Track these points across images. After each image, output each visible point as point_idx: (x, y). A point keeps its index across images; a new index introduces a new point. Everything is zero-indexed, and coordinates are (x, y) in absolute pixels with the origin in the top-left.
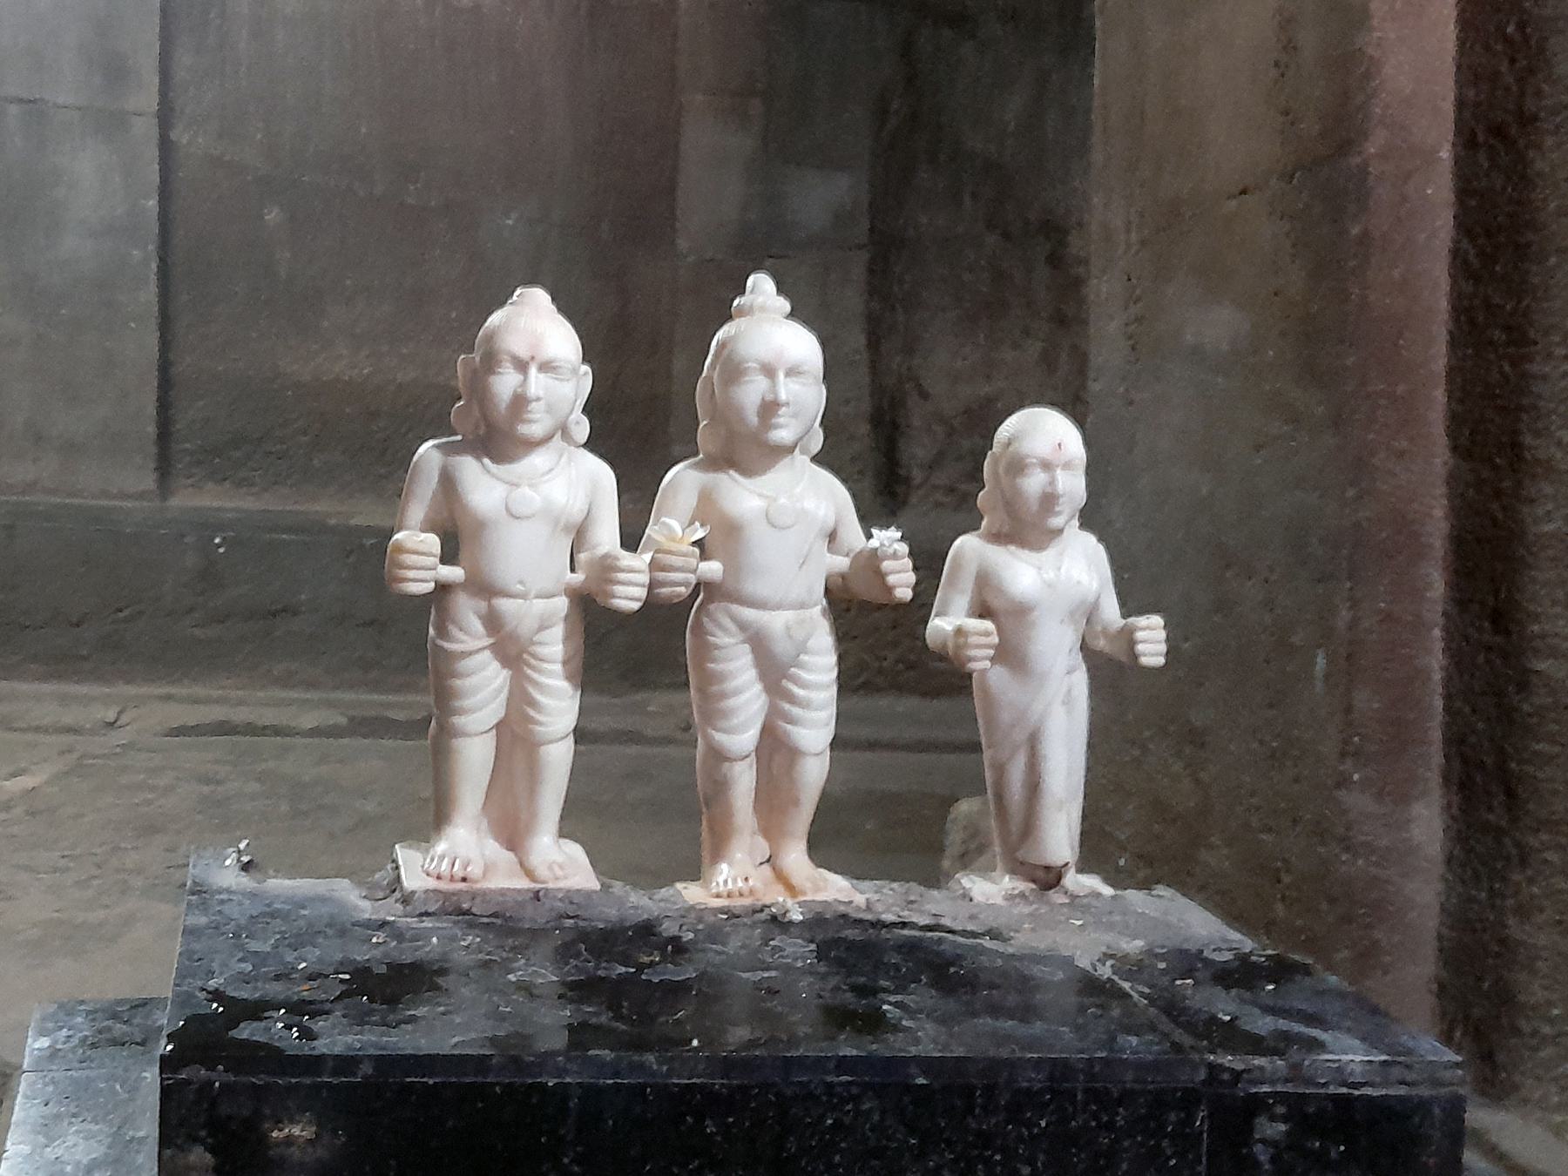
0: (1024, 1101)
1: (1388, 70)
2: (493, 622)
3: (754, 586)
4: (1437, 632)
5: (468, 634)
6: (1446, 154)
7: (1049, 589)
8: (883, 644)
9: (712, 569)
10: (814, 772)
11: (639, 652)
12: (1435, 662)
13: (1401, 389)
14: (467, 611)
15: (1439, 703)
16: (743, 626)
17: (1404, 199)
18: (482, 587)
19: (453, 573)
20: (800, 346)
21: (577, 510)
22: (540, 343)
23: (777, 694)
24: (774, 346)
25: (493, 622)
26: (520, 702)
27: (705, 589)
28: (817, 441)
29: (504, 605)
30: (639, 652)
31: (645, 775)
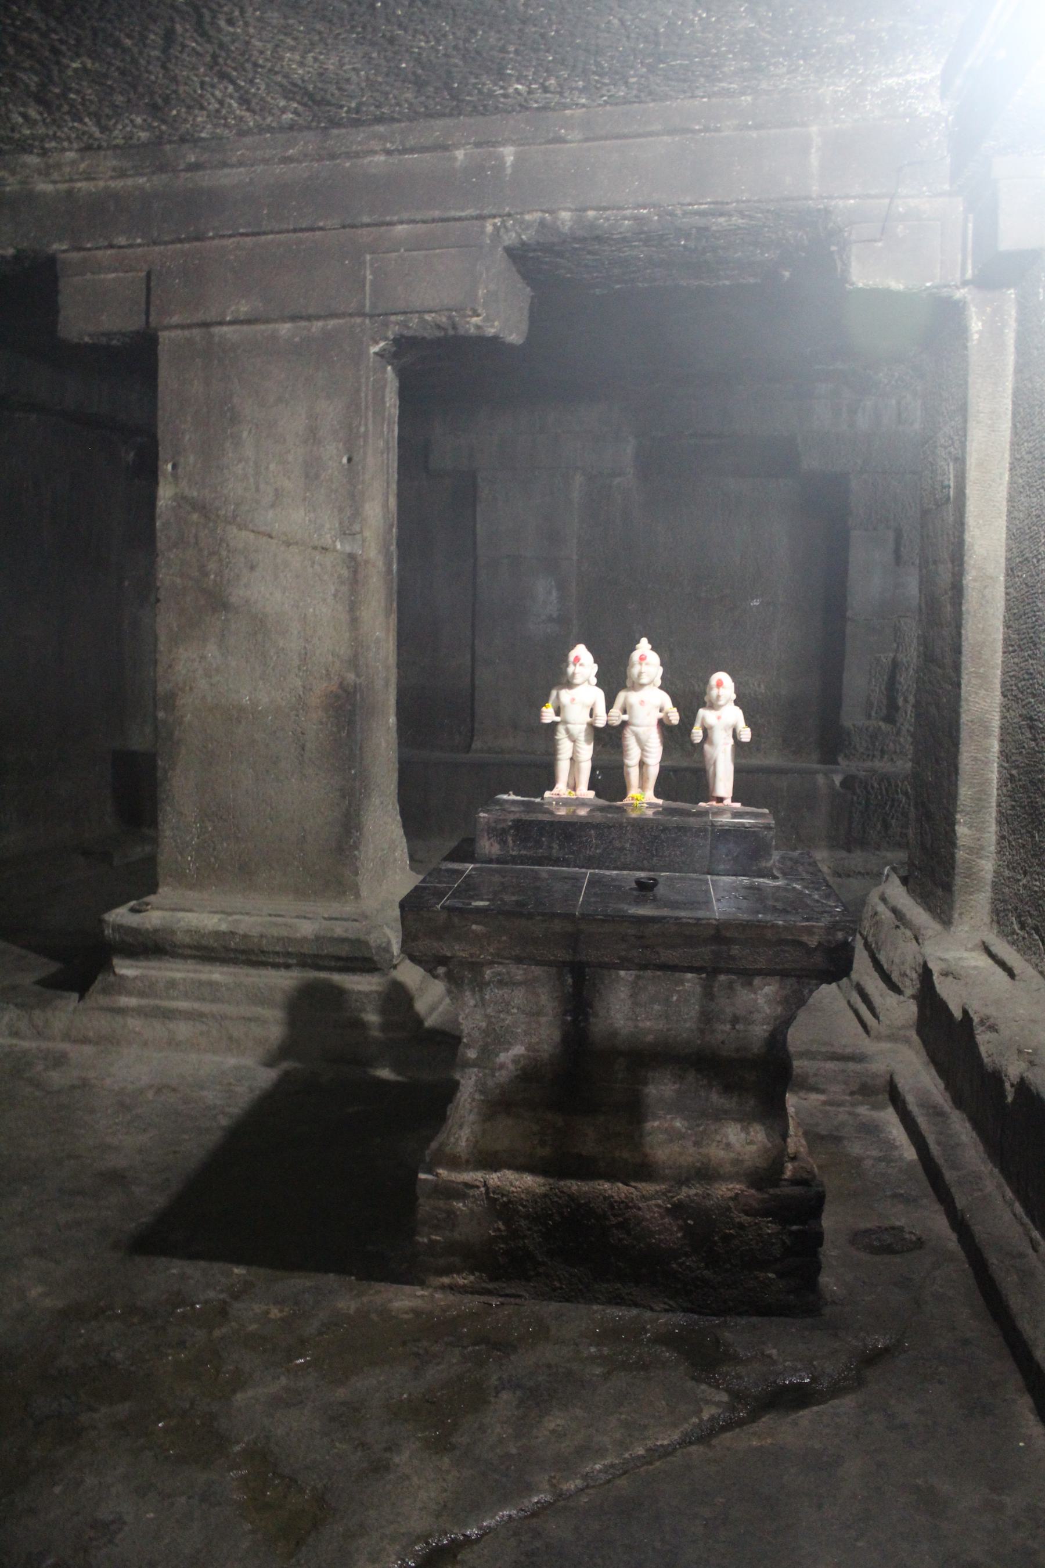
0: (115, 334)
1: (976, 547)
2: (567, 731)
3: (635, 721)
4: (996, 765)
5: (561, 735)
6: (1002, 578)
7: (724, 721)
8: (675, 736)
9: (625, 717)
10: (654, 771)
11: (609, 740)
12: (994, 776)
13: (982, 670)
14: (561, 729)
15: (995, 792)
16: (633, 732)
17: (984, 596)
18: (565, 722)
19: (558, 719)
20: (654, 658)
21: (590, 703)
22: (583, 663)
23: (645, 752)
24: (647, 661)
25: (567, 731)
26: (575, 752)
27: (624, 724)
28: (659, 682)
29: (569, 726)
30: (609, 740)
31: (609, 777)
